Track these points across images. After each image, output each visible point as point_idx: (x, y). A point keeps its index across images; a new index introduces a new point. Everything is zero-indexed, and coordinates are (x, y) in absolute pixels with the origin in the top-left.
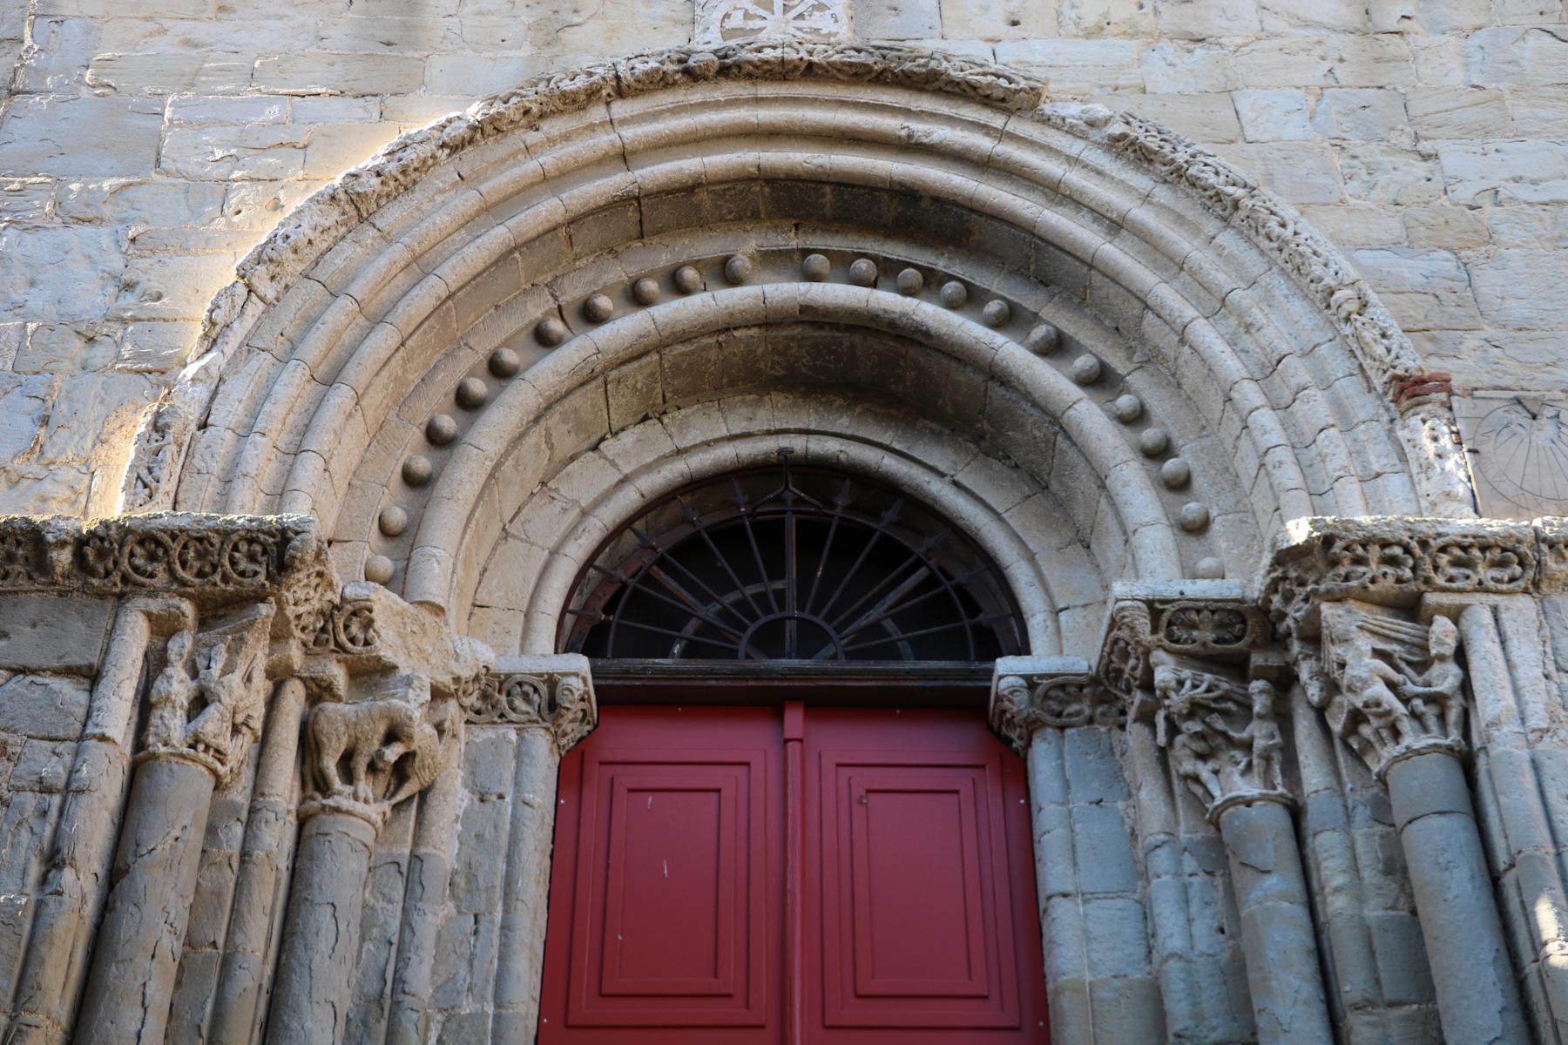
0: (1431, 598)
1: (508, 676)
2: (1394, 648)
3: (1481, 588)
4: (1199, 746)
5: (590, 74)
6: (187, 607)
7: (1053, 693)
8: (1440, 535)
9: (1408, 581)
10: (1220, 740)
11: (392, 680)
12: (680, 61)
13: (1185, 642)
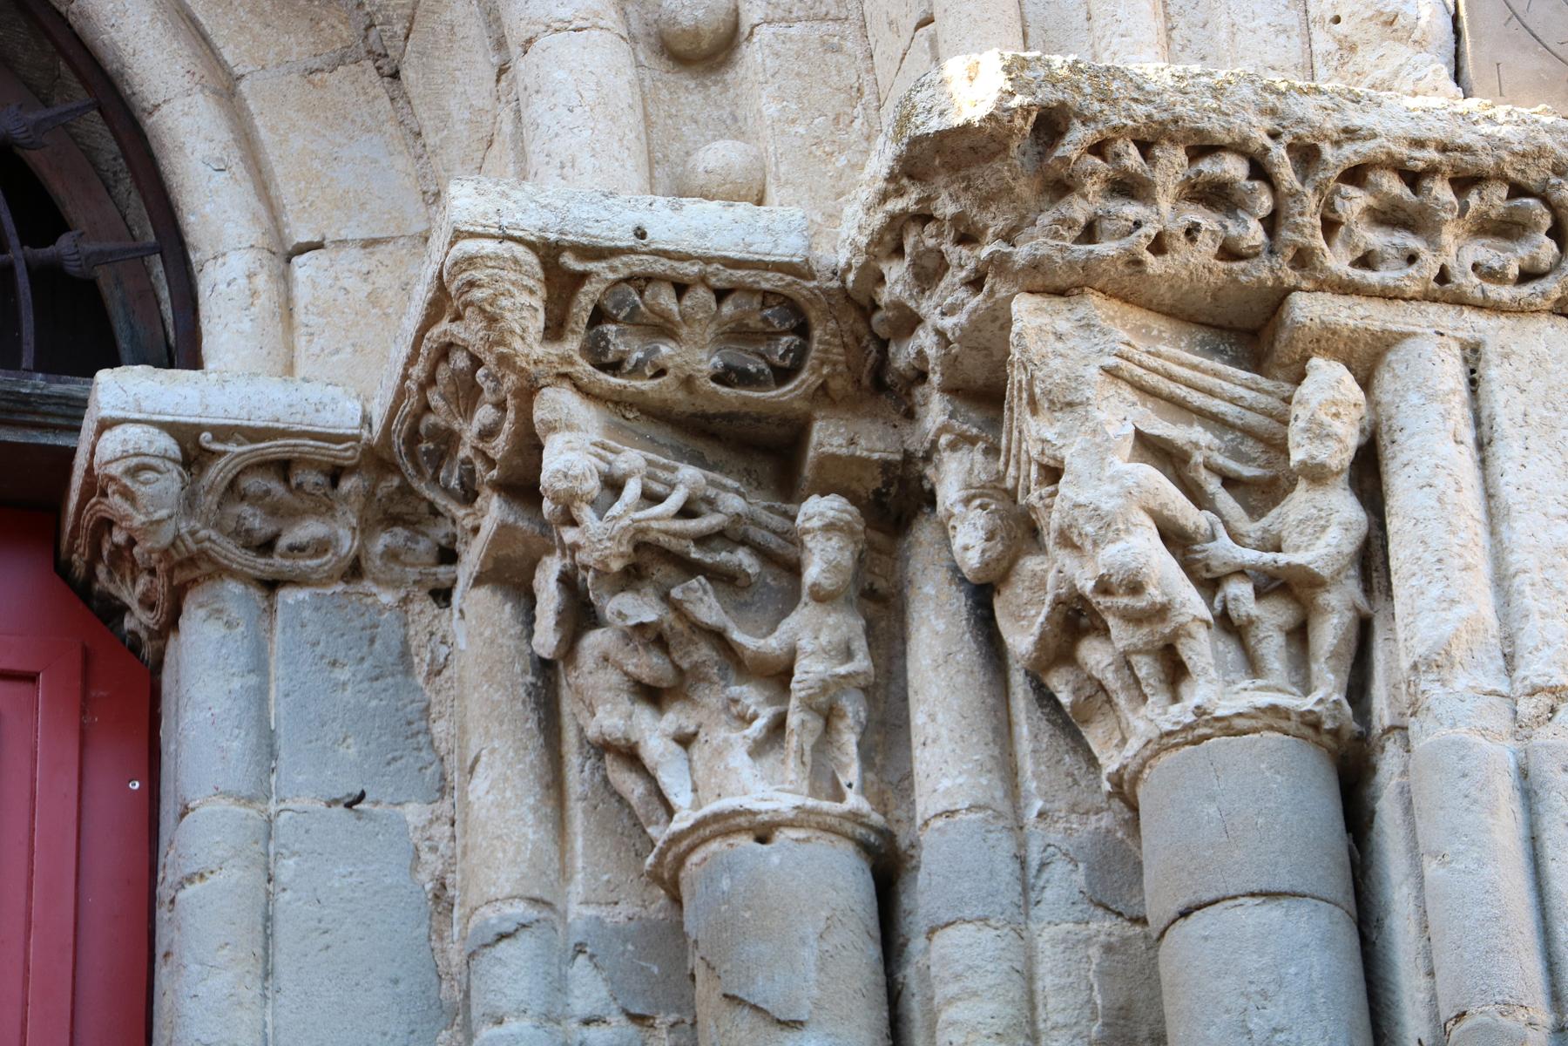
0: (1308, 308)
4: (650, 665)
7: (253, 483)
8: (1351, 134)
10: (704, 652)
13: (637, 371)
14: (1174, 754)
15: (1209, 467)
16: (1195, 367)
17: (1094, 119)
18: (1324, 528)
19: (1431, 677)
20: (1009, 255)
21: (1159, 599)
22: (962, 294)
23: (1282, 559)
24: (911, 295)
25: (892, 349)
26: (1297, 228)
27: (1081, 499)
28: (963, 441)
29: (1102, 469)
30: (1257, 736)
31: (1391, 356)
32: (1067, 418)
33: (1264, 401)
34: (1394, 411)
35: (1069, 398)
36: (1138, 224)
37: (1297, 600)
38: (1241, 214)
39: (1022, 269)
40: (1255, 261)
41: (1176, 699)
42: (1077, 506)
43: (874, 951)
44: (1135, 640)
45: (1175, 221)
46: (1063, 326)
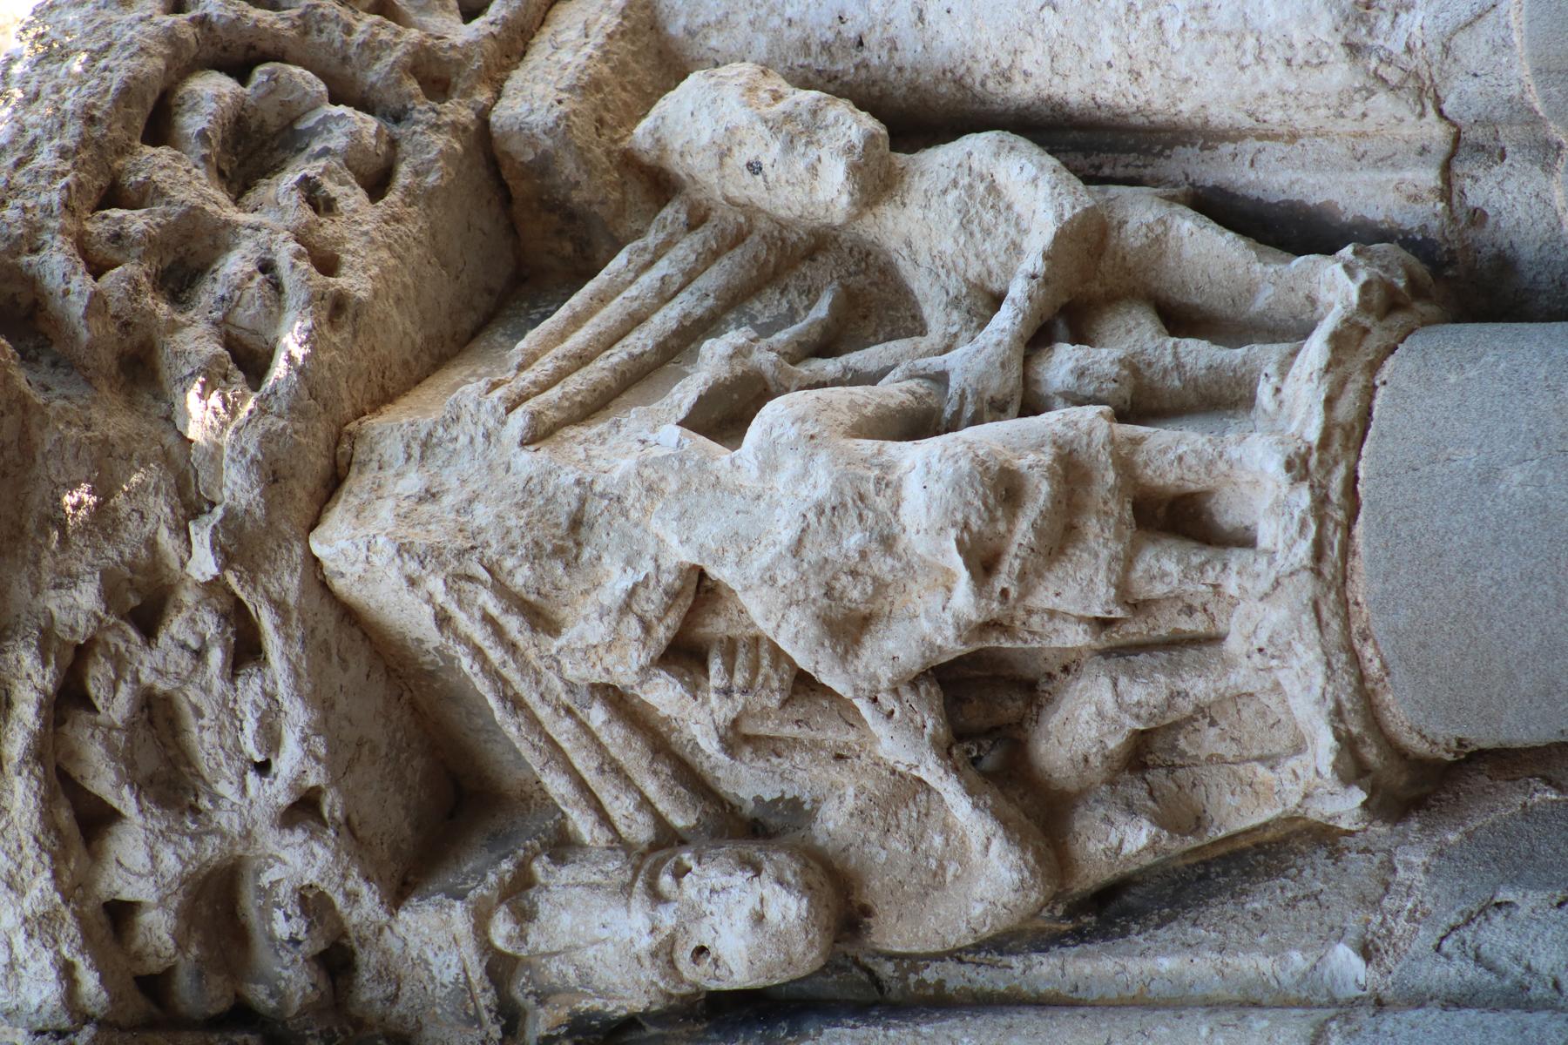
0: (534, 99)
2: (714, 359)
14: (1360, 564)
16: (576, 321)
17: (35, 229)
18: (993, 188)
19: (1385, 23)
20: (229, 514)
21: (1046, 458)
22: (250, 689)
23: (1018, 290)
24: (194, 837)
25: (259, 994)
26: (372, 48)
27: (786, 536)
28: (519, 894)
29: (737, 490)
30: (1381, 391)
31: (676, 28)
32: (603, 540)
33: (686, 250)
34: (795, 33)
35: (564, 520)
36: (266, 267)
37: (1114, 299)
38: (301, 126)
39: (269, 506)
40: (406, 146)
41: (1244, 540)
42: (797, 548)
44: (1104, 554)
45: (283, 210)
46: (413, 482)
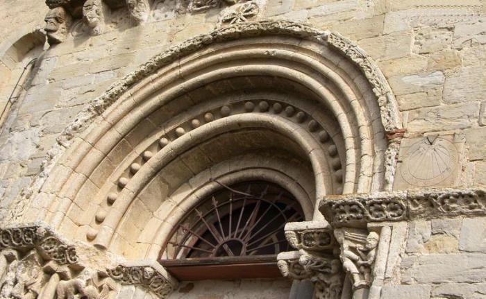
1: (131, 268)
3: (387, 220)
5: (172, 50)
6: (15, 253)
7: (296, 266)
8: (369, 199)
9: (361, 218)
11: (82, 272)
12: (201, 40)
15: (360, 250)
43: (118, 220)
